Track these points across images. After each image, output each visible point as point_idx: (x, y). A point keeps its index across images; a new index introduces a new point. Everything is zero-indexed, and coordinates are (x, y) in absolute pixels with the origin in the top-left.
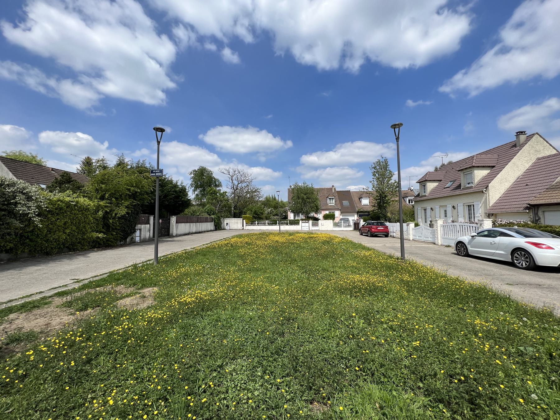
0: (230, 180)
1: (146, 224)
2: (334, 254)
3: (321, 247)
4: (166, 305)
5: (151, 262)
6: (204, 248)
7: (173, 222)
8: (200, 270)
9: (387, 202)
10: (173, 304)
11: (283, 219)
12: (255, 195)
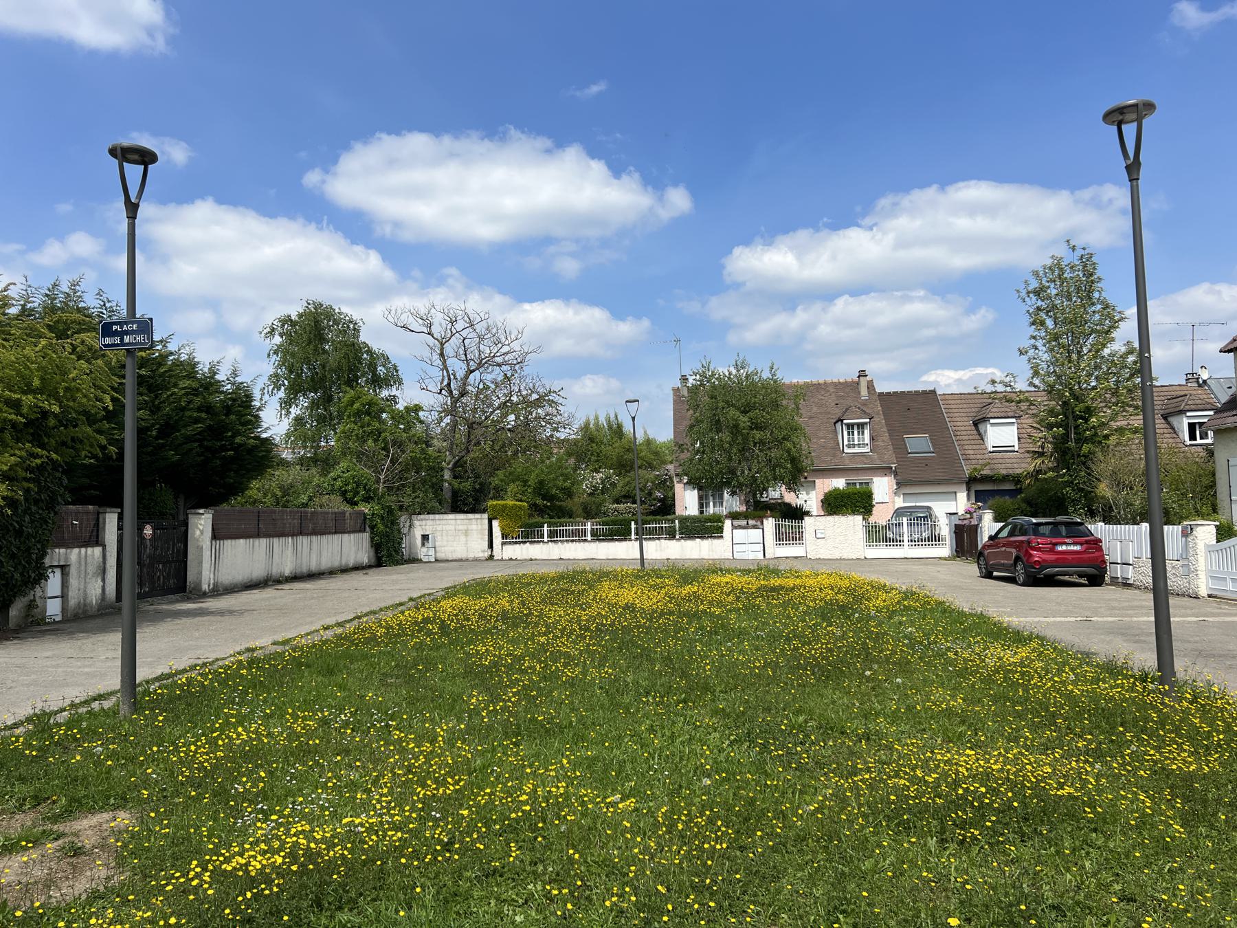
0: (436, 357)
1: (87, 544)
2: (869, 660)
3: (814, 628)
4: (167, 885)
5: (107, 704)
6: (327, 640)
7: (202, 532)
8: (310, 734)
9: (1096, 435)
10: (194, 883)
11: (653, 513)
12: (538, 418)
